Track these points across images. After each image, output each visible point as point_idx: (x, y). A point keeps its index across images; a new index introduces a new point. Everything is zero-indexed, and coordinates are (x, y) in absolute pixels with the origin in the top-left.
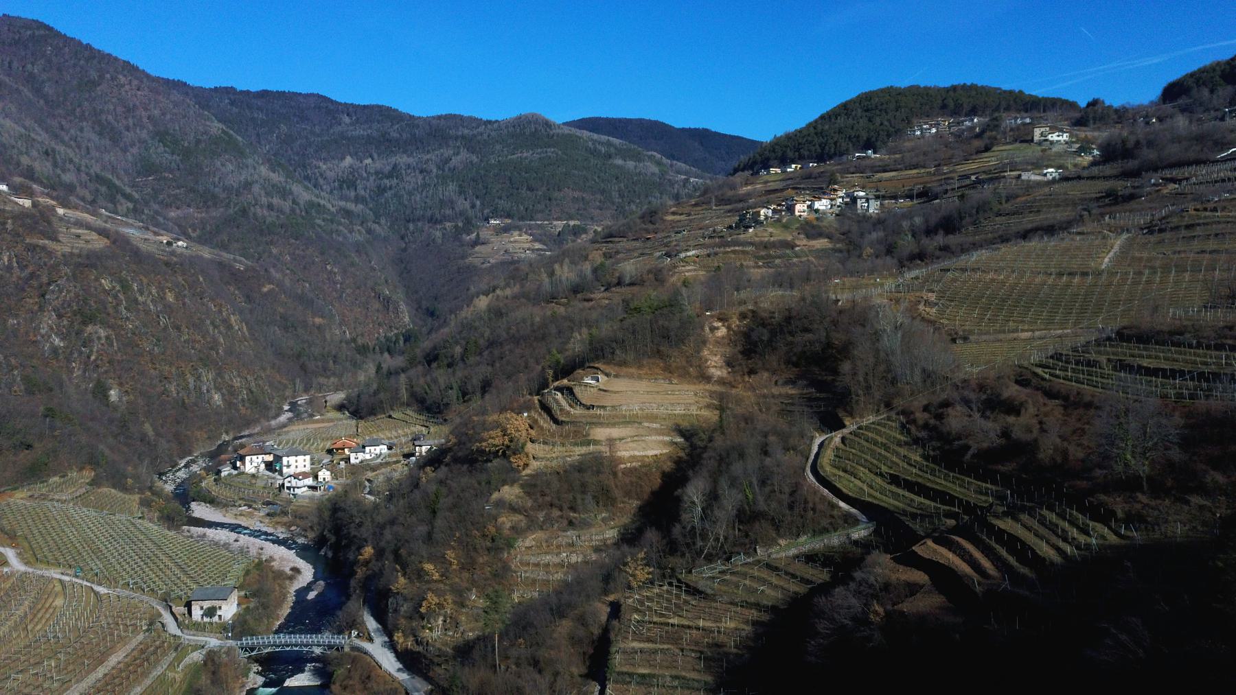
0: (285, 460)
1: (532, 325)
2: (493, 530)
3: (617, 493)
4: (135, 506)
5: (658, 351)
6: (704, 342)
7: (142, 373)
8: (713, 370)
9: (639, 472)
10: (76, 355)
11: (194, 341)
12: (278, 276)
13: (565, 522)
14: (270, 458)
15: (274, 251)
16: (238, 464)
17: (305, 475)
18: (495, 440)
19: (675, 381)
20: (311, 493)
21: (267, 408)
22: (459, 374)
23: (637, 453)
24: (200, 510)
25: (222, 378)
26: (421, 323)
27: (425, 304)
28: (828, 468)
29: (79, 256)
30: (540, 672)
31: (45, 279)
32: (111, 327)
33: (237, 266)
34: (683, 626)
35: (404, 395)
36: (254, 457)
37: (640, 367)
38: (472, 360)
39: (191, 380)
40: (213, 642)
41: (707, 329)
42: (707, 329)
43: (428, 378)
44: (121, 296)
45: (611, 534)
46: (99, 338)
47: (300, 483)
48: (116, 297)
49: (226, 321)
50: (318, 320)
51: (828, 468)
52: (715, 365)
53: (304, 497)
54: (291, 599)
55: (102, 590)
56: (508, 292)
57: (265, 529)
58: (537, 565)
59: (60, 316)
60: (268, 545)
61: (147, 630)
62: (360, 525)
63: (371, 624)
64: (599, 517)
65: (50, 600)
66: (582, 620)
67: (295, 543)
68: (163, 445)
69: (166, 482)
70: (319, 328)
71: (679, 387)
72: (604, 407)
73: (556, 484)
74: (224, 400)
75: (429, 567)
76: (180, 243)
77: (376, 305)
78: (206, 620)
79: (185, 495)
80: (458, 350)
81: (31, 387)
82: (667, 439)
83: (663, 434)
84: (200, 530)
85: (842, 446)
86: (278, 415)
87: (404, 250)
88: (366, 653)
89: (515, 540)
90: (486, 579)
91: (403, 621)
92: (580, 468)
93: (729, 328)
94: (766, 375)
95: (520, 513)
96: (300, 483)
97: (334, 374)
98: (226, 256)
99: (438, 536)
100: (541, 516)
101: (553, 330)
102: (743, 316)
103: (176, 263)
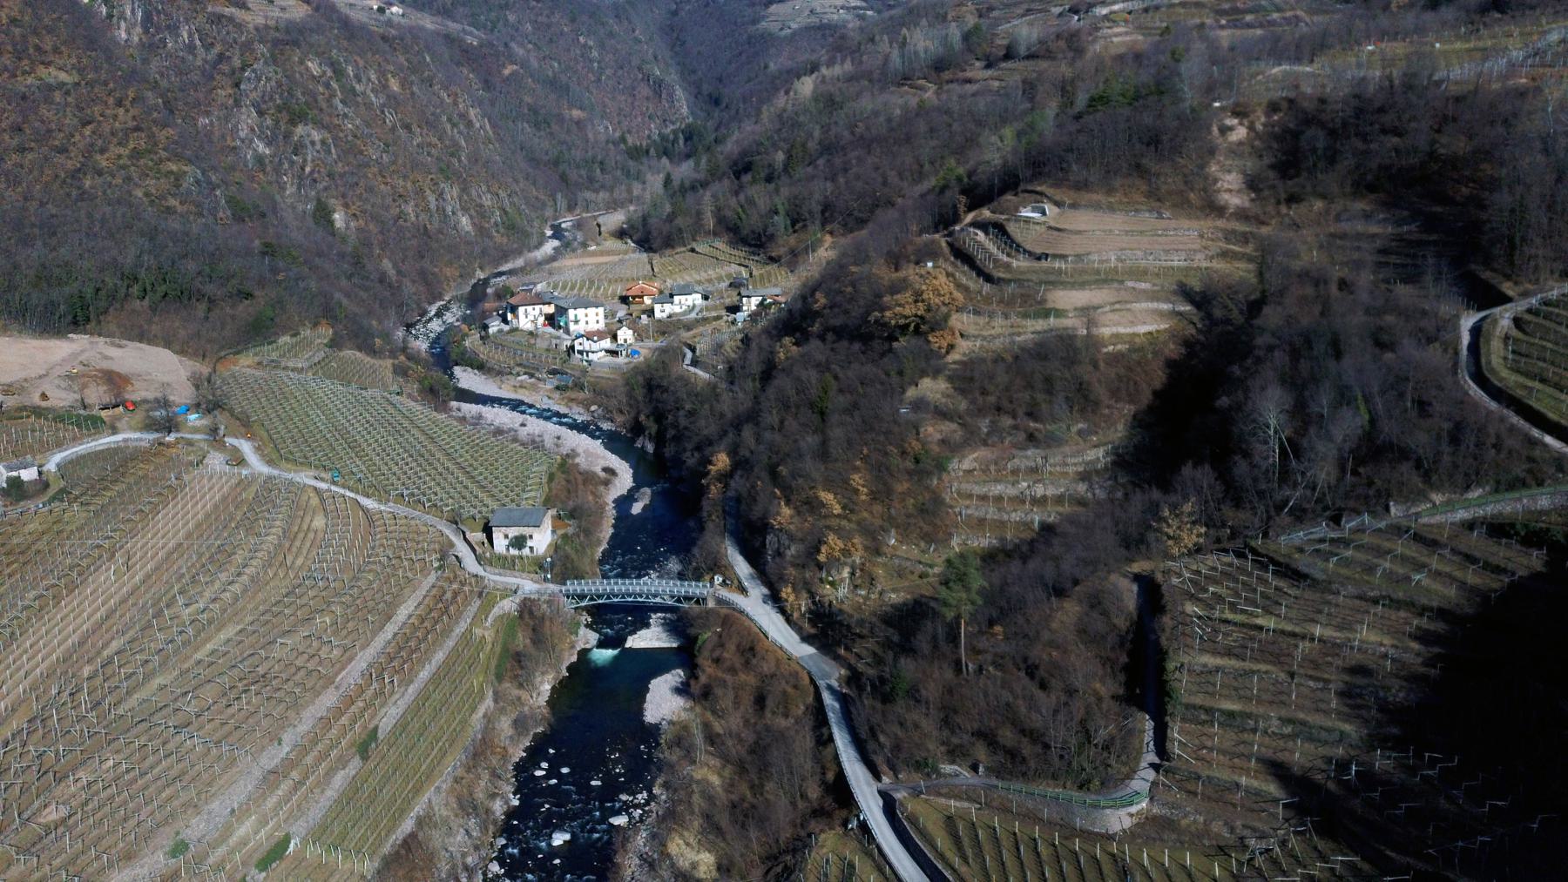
0: (571, 313)
1: (889, 120)
2: (916, 446)
3: (1100, 391)
4: (389, 374)
5: (1138, 166)
6: (1212, 152)
7: (370, 190)
8: (1225, 197)
9: (1130, 359)
10: (286, 166)
11: (430, 144)
12: (521, 52)
13: (1022, 436)
14: (550, 309)
15: (512, 18)
16: (509, 316)
17: (600, 335)
18: (903, 308)
19: (1167, 214)
20: (609, 359)
21: (528, 235)
22: (785, 192)
23: (1122, 330)
24: (467, 379)
25: (469, 195)
26: (703, 115)
27: (706, 88)
28: (1505, 373)
29: (277, 29)
30: (1043, 686)
31: (237, 63)
32: (327, 127)
33: (469, 39)
34: (1283, 632)
35: (710, 222)
36: (530, 308)
37: (1110, 191)
38: (801, 171)
39: (432, 199)
40: (528, 586)
41: (1215, 130)
42: (1215, 130)
43: (742, 197)
44: (334, 85)
45: (1097, 455)
46: (313, 143)
47: (595, 347)
48: (327, 86)
49: (463, 116)
50: (576, 113)
51: (1505, 373)
52: (1230, 187)
53: (602, 365)
54: (611, 512)
55: (369, 503)
56: (837, 70)
57: (555, 408)
58: (984, 498)
59: (261, 113)
60: (564, 431)
61: (439, 568)
62: (691, 413)
63: (742, 568)
64: (1074, 429)
65: (308, 519)
66: (1095, 602)
67: (599, 429)
68: (409, 288)
69: (417, 337)
70: (578, 123)
71: (1173, 223)
72: (1063, 257)
73: (1002, 378)
74: (474, 224)
75: (827, 497)
76: (395, 9)
77: (644, 91)
78: (513, 552)
79: (446, 355)
80: (780, 157)
81: (240, 213)
82: (1165, 307)
83: (1158, 300)
84: (470, 409)
85: (1515, 333)
86: (540, 245)
87: (675, 13)
88: (742, 612)
89: (948, 459)
90: (909, 516)
91: (791, 572)
92: (1041, 351)
93: (1251, 128)
94: (1319, 205)
95: (951, 420)
96: (595, 347)
97: (603, 187)
98: (453, 27)
99: (835, 450)
100: (984, 425)
101: (922, 127)
102: (1273, 107)
103: (394, 38)
